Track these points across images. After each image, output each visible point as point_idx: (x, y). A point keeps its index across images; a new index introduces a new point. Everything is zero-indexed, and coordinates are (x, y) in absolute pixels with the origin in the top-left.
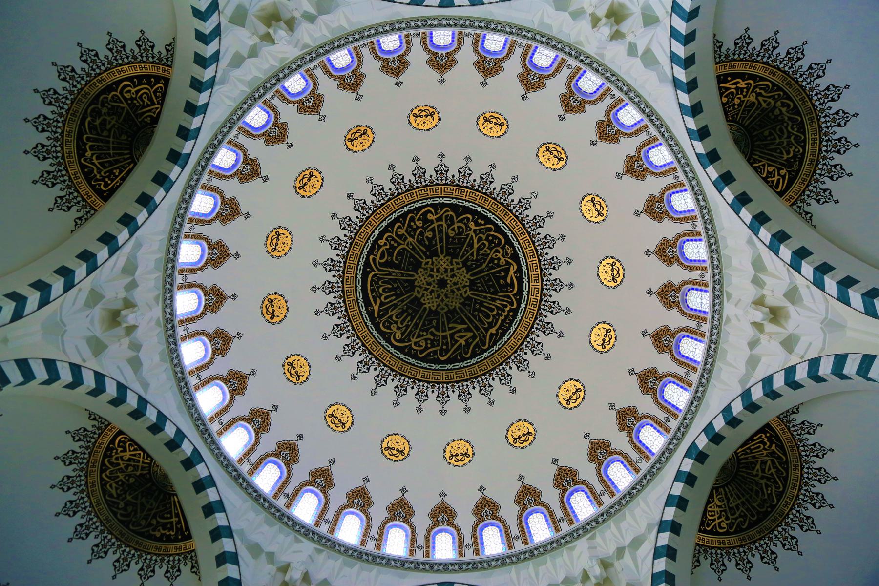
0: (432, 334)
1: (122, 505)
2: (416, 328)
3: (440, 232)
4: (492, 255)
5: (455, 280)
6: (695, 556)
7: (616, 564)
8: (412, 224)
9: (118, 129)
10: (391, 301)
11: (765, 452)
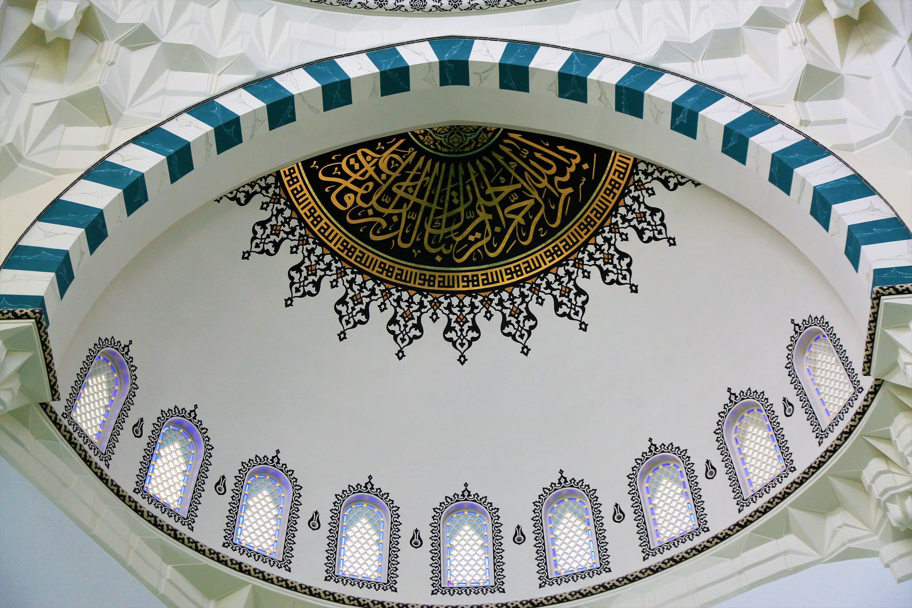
6: (252, 185)
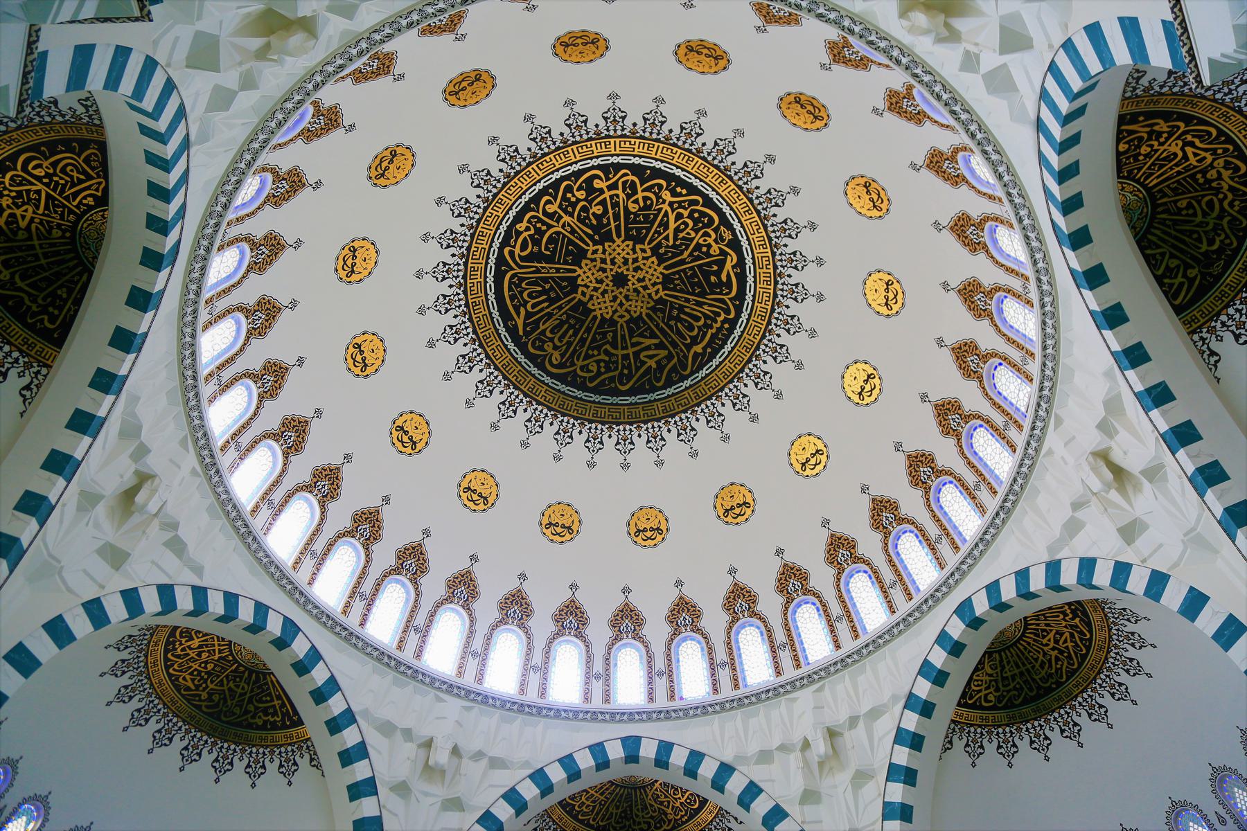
0: (607, 352)
1: (204, 695)
2: (582, 347)
3: (615, 205)
4: (699, 239)
5: (640, 275)
7: (847, 734)
8: (569, 195)
9: (41, 223)
10: (542, 310)
11: (1064, 623)
